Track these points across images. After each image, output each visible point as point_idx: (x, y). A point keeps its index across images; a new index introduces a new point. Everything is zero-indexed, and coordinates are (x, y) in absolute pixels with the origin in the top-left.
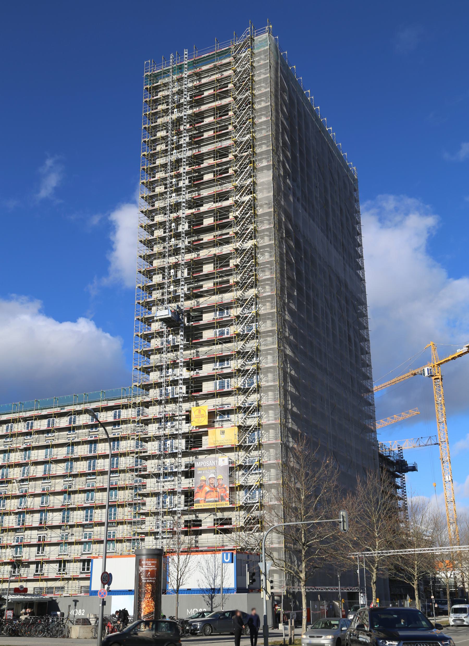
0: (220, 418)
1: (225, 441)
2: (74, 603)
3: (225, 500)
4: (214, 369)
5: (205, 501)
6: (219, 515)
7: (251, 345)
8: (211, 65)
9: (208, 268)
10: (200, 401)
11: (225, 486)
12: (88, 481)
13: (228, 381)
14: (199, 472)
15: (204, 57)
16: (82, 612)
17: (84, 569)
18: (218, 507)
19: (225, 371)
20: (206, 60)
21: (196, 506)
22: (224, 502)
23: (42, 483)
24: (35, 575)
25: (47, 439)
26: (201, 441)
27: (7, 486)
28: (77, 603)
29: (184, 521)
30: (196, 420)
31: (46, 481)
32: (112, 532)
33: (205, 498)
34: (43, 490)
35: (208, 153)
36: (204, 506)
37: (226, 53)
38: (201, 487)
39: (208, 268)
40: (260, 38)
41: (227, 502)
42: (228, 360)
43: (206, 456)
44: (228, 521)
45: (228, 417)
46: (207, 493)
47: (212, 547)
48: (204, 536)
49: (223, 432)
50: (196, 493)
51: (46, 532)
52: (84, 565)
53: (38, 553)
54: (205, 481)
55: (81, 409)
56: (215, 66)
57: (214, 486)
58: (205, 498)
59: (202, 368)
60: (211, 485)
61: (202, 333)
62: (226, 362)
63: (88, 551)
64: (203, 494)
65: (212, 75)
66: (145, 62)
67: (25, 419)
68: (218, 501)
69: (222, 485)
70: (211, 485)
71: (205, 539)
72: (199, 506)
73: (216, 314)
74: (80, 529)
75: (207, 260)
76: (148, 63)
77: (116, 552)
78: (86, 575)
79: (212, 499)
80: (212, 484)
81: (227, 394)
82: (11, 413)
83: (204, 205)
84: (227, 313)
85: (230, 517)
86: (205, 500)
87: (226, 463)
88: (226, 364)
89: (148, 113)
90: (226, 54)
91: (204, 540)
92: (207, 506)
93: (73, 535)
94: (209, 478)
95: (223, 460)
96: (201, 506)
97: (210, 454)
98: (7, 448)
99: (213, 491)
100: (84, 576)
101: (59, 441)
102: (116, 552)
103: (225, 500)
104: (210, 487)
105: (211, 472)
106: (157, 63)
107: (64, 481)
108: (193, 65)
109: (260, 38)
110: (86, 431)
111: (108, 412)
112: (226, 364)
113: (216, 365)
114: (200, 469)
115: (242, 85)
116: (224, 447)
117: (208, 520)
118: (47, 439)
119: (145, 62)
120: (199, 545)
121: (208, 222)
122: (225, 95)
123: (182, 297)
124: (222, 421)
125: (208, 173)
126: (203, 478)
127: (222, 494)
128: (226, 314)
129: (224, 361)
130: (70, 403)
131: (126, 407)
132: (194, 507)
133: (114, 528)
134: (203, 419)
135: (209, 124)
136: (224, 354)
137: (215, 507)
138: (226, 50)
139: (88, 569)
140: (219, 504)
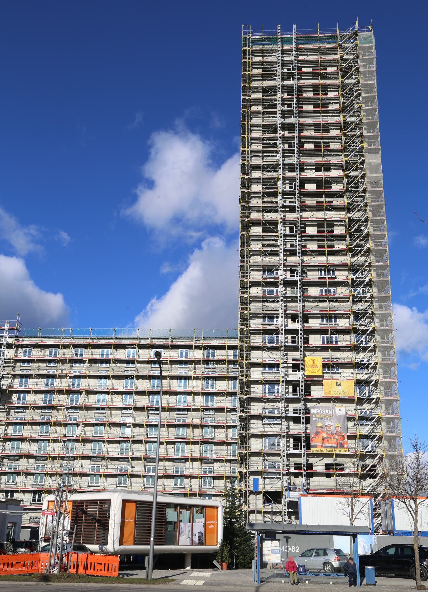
0: (268, 370)
1: (342, 393)
2: (285, 539)
3: (344, 447)
4: (321, 324)
5: (322, 446)
6: (330, 460)
7: (359, 307)
8: (316, 46)
9: (312, 230)
10: (307, 352)
11: (343, 434)
12: (150, 415)
13: (336, 337)
14: (315, 419)
15: (307, 37)
16: (296, 549)
17: (34, 500)
18: (336, 453)
19: (269, 327)
20: (313, 39)
21: (313, 451)
22: (343, 449)
23: (95, 413)
24: (31, 504)
25: (100, 369)
26: (310, 389)
27: (51, 412)
28: (289, 540)
29: (293, 464)
30: (310, 369)
31: (100, 412)
32: (123, 466)
33: (323, 443)
34: (43, 419)
35: (309, 125)
36: (321, 451)
37: (330, 39)
38: (317, 433)
39: (339, 230)
40: (364, 35)
41: (345, 449)
42: (335, 318)
43: (316, 404)
44: (340, 467)
45: (338, 370)
46: (323, 439)
47: (331, 490)
48: (315, 479)
49: (339, 384)
50: (313, 438)
51: (100, 463)
52: (34, 496)
53: (176, 485)
54: (322, 427)
55: (145, 344)
56: (319, 48)
57: (332, 433)
58: (323, 443)
59: (308, 321)
60: (328, 432)
61: (307, 289)
62: (275, 319)
63: (96, 483)
64: (320, 440)
65: (310, 55)
66: (243, 26)
67: (75, 346)
68: (337, 447)
69: (340, 433)
70: (328, 432)
71: (317, 482)
72: (316, 451)
73: (321, 273)
74: (143, 462)
75: (312, 223)
76: (245, 27)
77: (184, 488)
78: (35, 506)
79: (330, 445)
80: (330, 431)
81: (336, 349)
82: (60, 338)
83: (305, 171)
84: (333, 275)
85: (343, 463)
86: (322, 446)
87: (343, 413)
88: (275, 321)
89: (247, 73)
90: (333, 39)
91: (316, 483)
92: (325, 451)
93: (134, 467)
94: (326, 426)
95: (340, 410)
96: (318, 451)
97: (319, 403)
98: (51, 373)
99: (330, 438)
100: (33, 506)
101: (116, 373)
102: (184, 488)
103: (344, 447)
104: (327, 433)
105: (328, 419)
106: (256, 29)
107: (177, 414)
108: (300, 40)
109: (364, 35)
110: (148, 366)
111: (173, 350)
112: (275, 321)
113: (323, 321)
114: (315, 416)
115: (351, 71)
116: (340, 397)
117: (319, 464)
118: (100, 369)
119: (243, 26)
120: (311, 487)
121: (311, 187)
122: (272, 77)
123: (281, 253)
124: (332, 373)
125: (309, 143)
126: (320, 424)
127: (341, 441)
128: (331, 275)
129: (274, 318)
130: (35, 335)
131: (65, 347)
132: (311, 451)
133: (212, 465)
134: (318, 369)
135: (309, 99)
136: (336, 312)
137: (333, 452)
138: (329, 36)
139: (39, 500)
140: (337, 451)
